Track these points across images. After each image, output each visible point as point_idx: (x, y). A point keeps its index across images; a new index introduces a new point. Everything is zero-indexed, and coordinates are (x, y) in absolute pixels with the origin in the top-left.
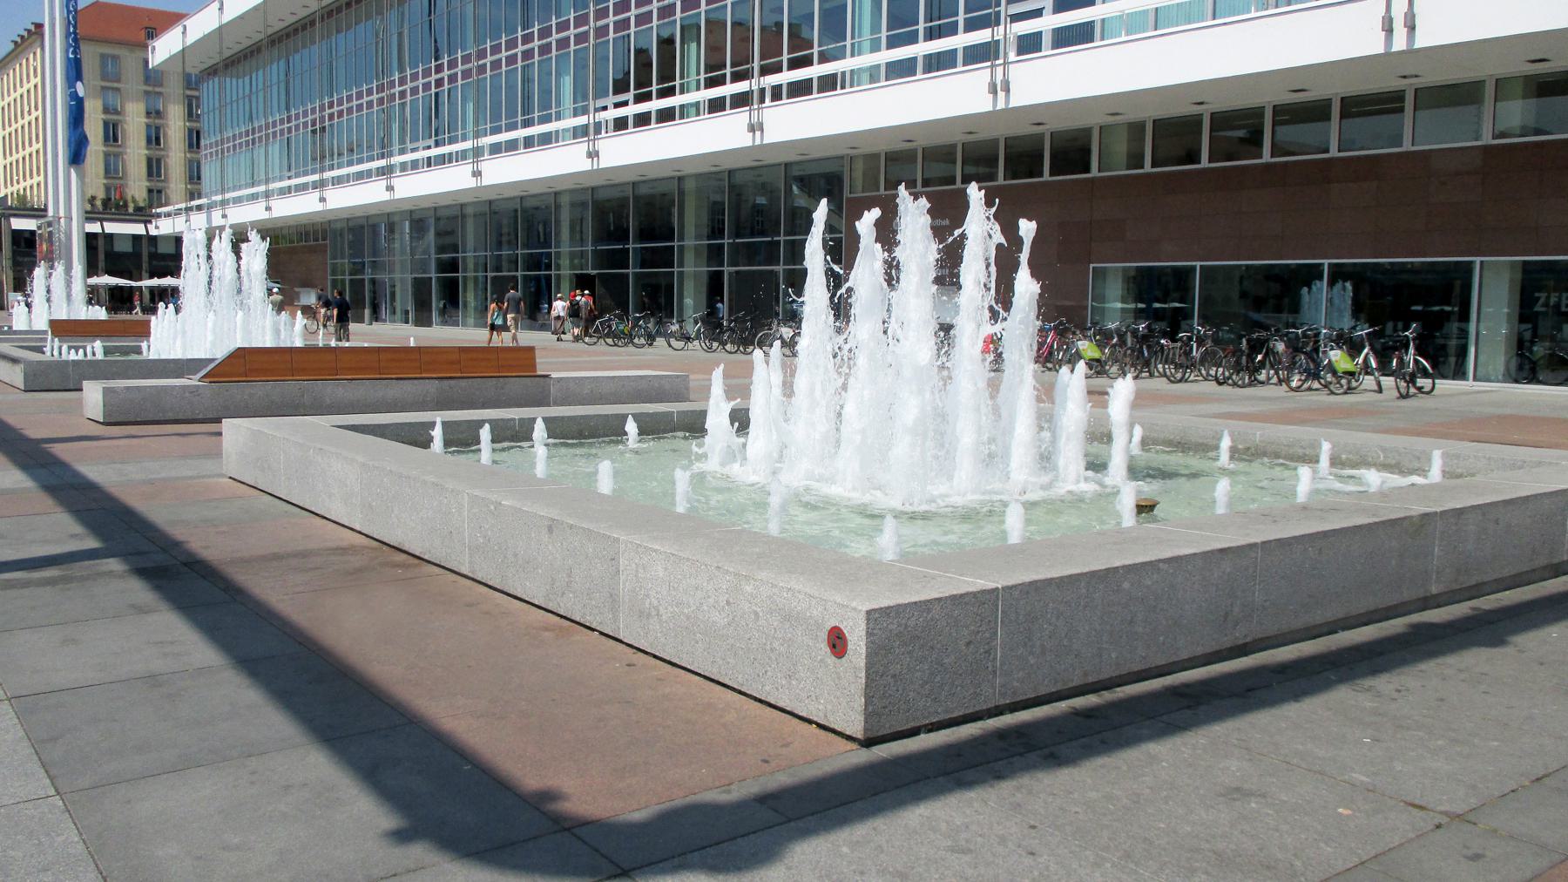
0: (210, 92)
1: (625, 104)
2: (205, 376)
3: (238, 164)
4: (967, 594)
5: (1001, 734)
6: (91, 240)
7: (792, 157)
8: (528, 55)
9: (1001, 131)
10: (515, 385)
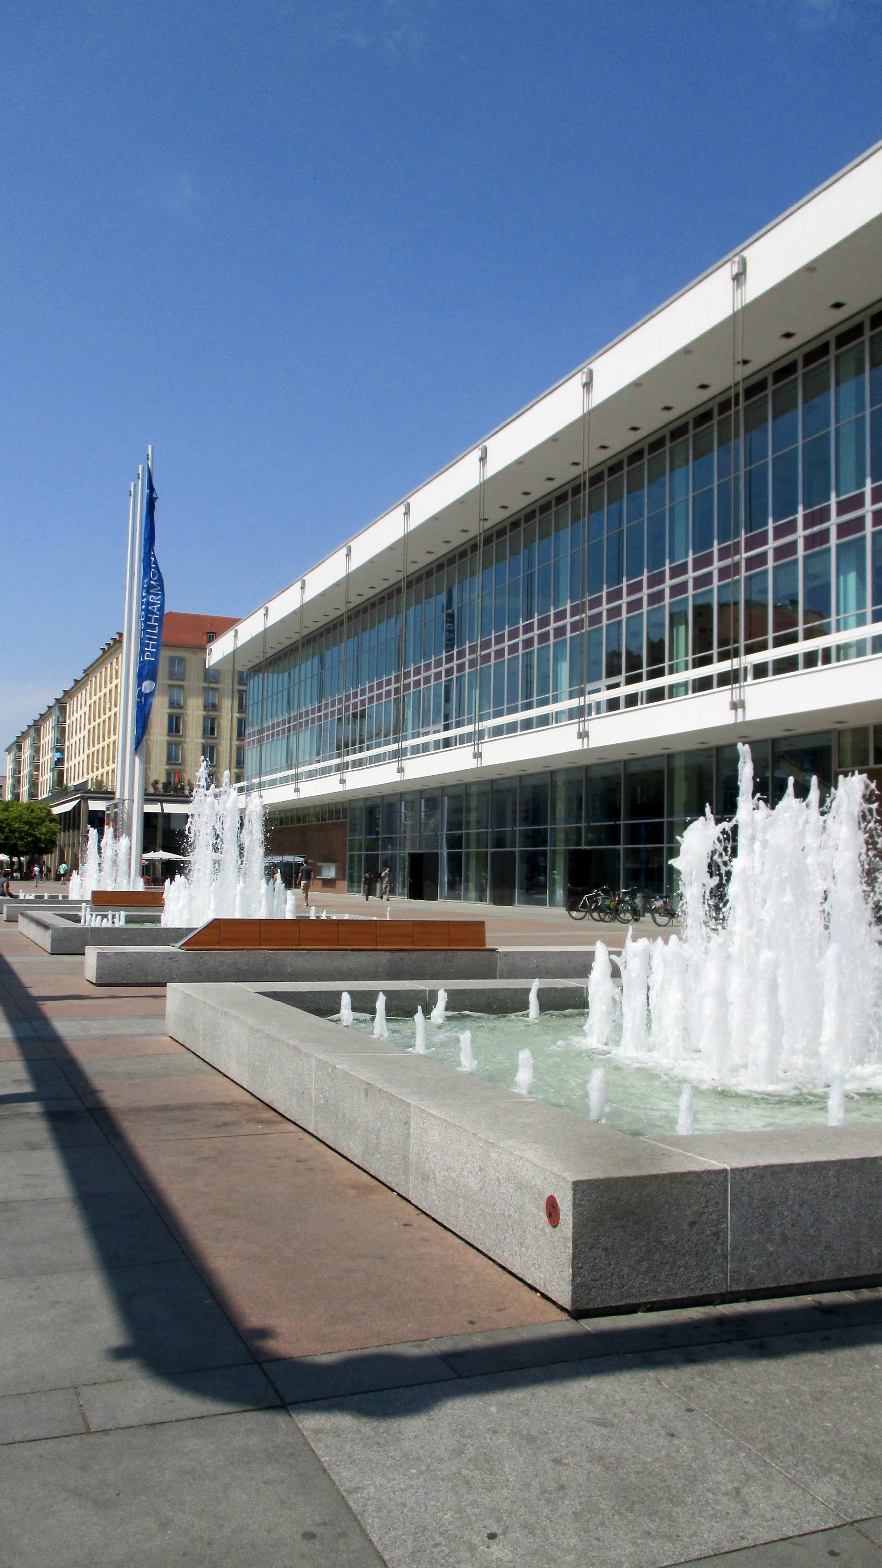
0: (254, 685)
1: (617, 685)
2: (183, 945)
3: (276, 750)
4: (689, 1173)
5: (722, 1321)
6: (149, 820)
7: (777, 733)
8: (528, 643)
10: (464, 958)
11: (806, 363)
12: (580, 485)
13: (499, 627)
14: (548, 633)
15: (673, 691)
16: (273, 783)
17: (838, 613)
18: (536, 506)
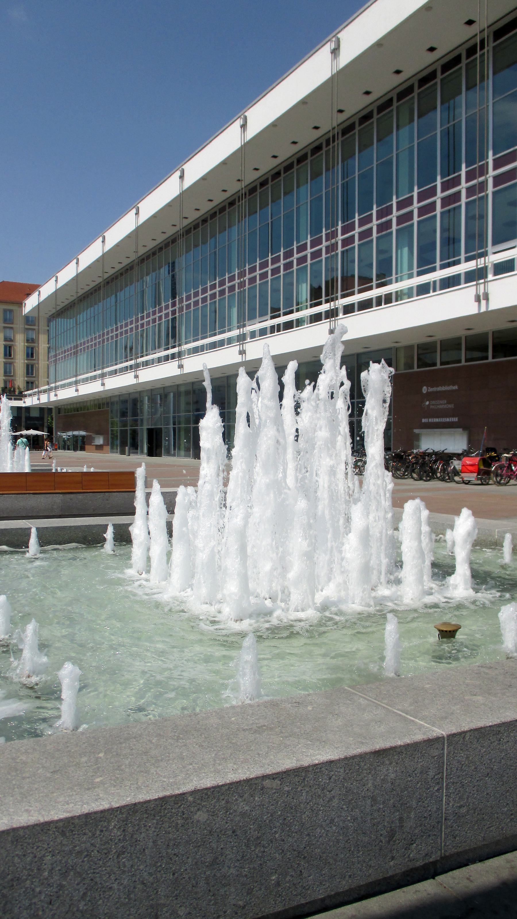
9: (489, 327)
11: (360, 124)
12: (476, 45)
13: (196, 287)
14: (225, 289)
15: (299, 322)
16: (63, 386)
17: (397, 274)
18: (217, 209)
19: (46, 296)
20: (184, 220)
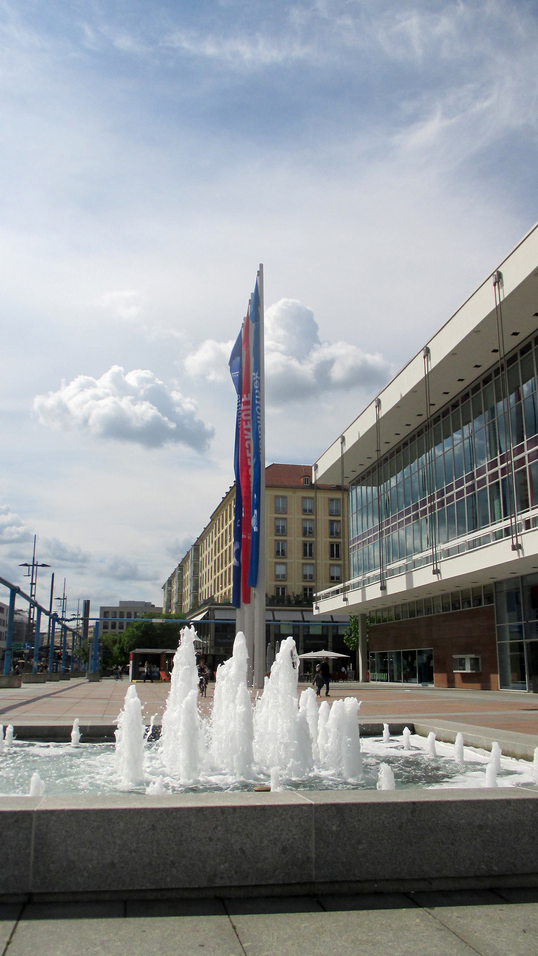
12: (499, 368)
19: (319, 476)
20: (431, 407)
